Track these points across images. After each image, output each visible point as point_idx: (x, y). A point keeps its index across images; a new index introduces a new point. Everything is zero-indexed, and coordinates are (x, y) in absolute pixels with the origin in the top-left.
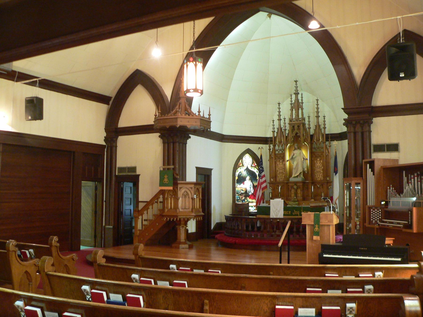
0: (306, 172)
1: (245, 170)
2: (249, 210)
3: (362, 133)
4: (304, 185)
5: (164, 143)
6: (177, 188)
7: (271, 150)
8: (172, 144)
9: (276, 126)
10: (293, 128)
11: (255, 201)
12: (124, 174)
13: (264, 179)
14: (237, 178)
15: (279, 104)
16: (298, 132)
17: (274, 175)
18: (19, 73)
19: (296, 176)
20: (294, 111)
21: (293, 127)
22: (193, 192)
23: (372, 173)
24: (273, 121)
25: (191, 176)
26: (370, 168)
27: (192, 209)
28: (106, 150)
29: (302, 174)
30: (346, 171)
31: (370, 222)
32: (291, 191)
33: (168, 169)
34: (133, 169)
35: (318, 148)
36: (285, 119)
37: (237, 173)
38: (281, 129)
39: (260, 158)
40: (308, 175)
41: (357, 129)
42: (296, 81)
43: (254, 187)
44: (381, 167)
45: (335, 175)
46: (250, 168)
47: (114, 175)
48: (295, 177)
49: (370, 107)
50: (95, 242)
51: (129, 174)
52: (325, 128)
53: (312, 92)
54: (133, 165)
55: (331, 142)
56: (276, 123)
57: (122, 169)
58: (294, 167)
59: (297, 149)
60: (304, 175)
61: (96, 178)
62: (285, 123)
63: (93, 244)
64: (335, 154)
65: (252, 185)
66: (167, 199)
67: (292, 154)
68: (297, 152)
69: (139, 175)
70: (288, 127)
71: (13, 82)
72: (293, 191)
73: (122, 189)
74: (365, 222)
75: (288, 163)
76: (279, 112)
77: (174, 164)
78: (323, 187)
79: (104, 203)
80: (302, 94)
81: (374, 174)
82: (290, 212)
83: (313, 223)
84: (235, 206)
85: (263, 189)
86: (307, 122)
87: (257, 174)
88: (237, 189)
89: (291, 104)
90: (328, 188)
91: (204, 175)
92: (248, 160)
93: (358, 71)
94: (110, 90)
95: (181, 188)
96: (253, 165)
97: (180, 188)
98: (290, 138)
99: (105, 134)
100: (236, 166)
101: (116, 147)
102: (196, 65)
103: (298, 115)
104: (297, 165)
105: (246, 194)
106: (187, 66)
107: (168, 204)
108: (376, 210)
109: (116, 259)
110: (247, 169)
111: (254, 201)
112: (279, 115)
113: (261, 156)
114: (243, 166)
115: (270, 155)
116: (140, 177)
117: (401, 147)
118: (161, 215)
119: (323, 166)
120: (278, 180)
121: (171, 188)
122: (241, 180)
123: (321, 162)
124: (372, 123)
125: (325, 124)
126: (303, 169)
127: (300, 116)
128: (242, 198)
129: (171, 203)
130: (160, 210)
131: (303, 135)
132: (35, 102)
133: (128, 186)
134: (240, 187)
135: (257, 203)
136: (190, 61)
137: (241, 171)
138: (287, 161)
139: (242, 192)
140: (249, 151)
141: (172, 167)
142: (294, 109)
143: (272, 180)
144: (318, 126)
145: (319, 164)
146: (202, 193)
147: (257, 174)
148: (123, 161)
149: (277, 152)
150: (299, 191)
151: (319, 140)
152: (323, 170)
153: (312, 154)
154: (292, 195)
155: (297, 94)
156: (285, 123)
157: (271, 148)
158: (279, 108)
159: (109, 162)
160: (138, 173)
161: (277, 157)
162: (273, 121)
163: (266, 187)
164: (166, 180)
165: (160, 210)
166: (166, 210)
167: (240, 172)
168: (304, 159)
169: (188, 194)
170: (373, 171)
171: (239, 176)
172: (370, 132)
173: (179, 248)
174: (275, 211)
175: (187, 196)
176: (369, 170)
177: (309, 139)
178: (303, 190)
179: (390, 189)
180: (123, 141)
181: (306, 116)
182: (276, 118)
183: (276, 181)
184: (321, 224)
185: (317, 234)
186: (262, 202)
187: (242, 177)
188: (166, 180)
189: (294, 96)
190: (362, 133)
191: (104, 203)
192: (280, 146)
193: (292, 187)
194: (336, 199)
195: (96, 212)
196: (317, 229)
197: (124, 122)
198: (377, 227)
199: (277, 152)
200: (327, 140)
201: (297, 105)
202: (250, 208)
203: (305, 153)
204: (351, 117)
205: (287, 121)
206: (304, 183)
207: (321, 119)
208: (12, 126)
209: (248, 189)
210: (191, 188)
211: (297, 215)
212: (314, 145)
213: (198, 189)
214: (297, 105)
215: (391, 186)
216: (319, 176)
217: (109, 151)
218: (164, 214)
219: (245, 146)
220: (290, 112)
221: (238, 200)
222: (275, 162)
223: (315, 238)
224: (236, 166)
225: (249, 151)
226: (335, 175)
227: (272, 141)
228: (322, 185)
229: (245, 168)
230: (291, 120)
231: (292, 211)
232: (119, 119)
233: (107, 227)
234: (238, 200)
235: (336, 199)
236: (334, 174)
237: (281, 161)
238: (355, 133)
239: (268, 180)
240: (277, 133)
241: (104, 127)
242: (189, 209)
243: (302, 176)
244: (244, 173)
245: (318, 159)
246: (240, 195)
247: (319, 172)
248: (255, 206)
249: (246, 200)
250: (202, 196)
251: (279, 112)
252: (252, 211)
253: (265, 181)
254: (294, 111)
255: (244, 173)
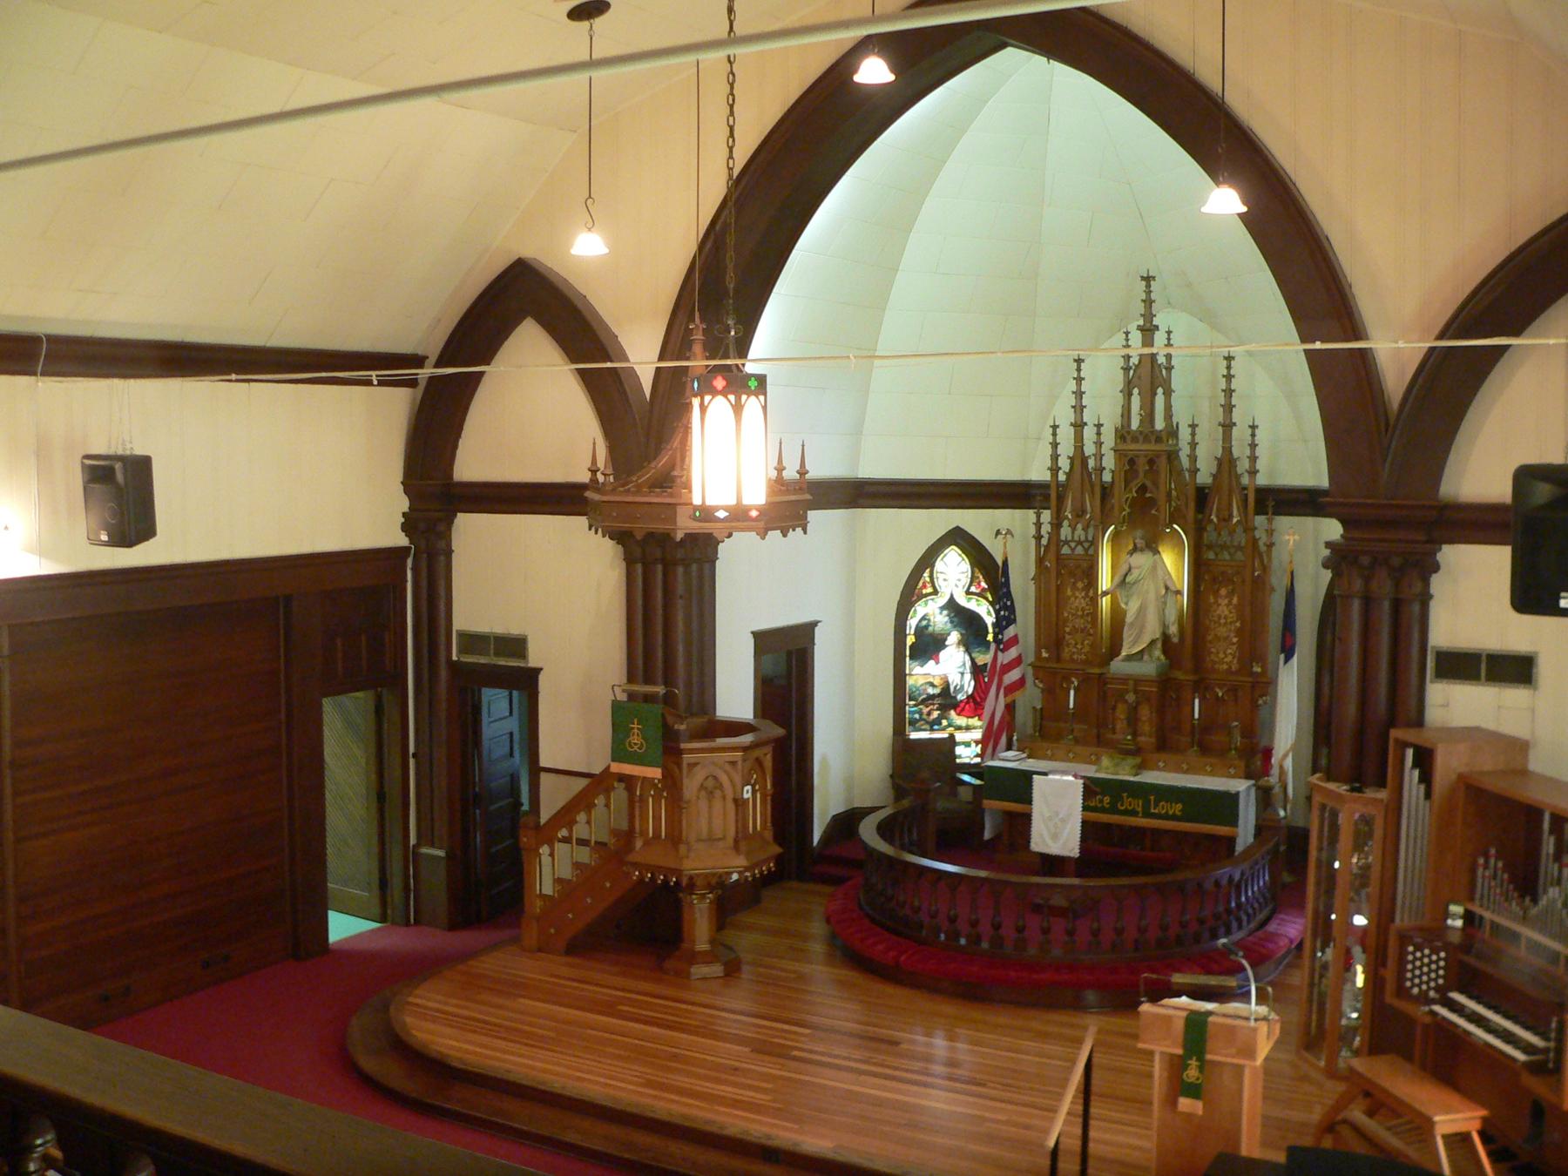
0: (1175, 640)
1: (942, 608)
2: (955, 757)
3: (1397, 606)
4: (1166, 691)
5: (629, 560)
6: (679, 765)
7: (1044, 541)
8: (660, 567)
9: (1066, 449)
10: (1128, 464)
11: (979, 723)
12: (483, 660)
13: (1013, 653)
14: (910, 640)
15: (1079, 361)
16: (1148, 484)
17: (1052, 635)
18: (50, 338)
19: (1137, 659)
20: (1136, 401)
21: (1132, 462)
22: (738, 779)
23: (1422, 787)
24: (1055, 427)
25: (735, 694)
26: (1415, 765)
27: (736, 841)
28: (409, 562)
29: (1159, 645)
30: (1329, 638)
31: (1402, 992)
32: (1114, 708)
33: (648, 698)
34: (516, 645)
35: (1224, 547)
36: (1099, 426)
37: (912, 623)
38: (1084, 460)
39: (1000, 563)
40: (1185, 649)
41: (1374, 585)
42: (1148, 279)
43: (977, 671)
44: (1461, 777)
45: (1286, 661)
46: (962, 600)
47: (443, 659)
48: (1129, 658)
49: (1431, 508)
50: (384, 903)
51: (502, 662)
52: (1253, 472)
53: (1209, 317)
54: (514, 630)
55: (1278, 518)
56: (1066, 436)
57: (473, 641)
58: (1129, 618)
59: (1142, 550)
60: (1165, 652)
61: (381, 676)
62: (1099, 444)
63: (376, 910)
64: (1286, 581)
65: (968, 664)
66: (643, 800)
67: (1125, 568)
68: (1142, 560)
69: (537, 671)
70: (1109, 462)
71: (33, 378)
72: (1121, 712)
73: (477, 709)
74: (1384, 965)
75: (1105, 602)
76: (1079, 394)
77: (668, 681)
78: (1236, 701)
79: (412, 761)
80: (1169, 333)
81: (1428, 795)
82: (1107, 799)
83: (1180, 1051)
84: (904, 751)
85: (1011, 689)
86: (1184, 453)
87: (990, 620)
88: (910, 681)
89: (1126, 369)
90: (1255, 706)
91: (787, 661)
92: (953, 570)
93: (1397, 346)
94: (417, 319)
95: (696, 764)
96: (973, 589)
97: (692, 765)
98: (1122, 499)
99: (404, 504)
100: (910, 595)
101: (449, 552)
102: (738, 409)
103: (1149, 416)
104: (1142, 610)
105: (946, 699)
106: (703, 409)
107: (644, 819)
108: (1427, 951)
109: (450, 1068)
110: (952, 605)
111: (975, 721)
112: (1079, 408)
113: (1005, 562)
114: (935, 592)
115: (1040, 561)
116: (542, 678)
117: (1543, 670)
118: (616, 851)
119: (1241, 617)
120: (1066, 654)
121: (655, 773)
122: (928, 646)
123: (1235, 600)
124: (1436, 568)
125: (1253, 459)
126: (1165, 626)
127: (1160, 424)
128: (929, 714)
129: (657, 818)
130: (615, 833)
131: (1169, 494)
132: (120, 477)
133: (496, 702)
134: (922, 675)
135: (983, 742)
136: (714, 392)
137: (930, 611)
138: (1105, 594)
139: (931, 691)
140: (958, 537)
141: (660, 690)
142: (1136, 391)
143: (1045, 655)
144: (1226, 462)
145: (1224, 608)
146: (775, 769)
147: (990, 620)
148: (477, 605)
149: (1065, 550)
150: (1145, 713)
151: (1231, 516)
152: (1239, 632)
153: (1199, 568)
154: (1119, 726)
155: (1148, 331)
156: (1099, 444)
157: (1043, 532)
158: (1079, 380)
159: (424, 609)
160: (533, 662)
161: (1066, 570)
162: (1055, 427)
163: (1021, 683)
164: (636, 739)
165: (615, 833)
166: (639, 844)
167: (923, 618)
168: (1167, 588)
169: (721, 787)
170: (1426, 778)
171: (920, 631)
172: (1425, 598)
173: (688, 976)
174: (1050, 819)
175: (718, 793)
176: (1412, 776)
177: (1191, 513)
178: (1161, 711)
179: (1486, 866)
180: (473, 532)
181: (1182, 418)
182: (1065, 417)
183: (1059, 659)
184: (1209, 1057)
185: (1194, 1091)
186: (1004, 739)
187: (932, 635)
188: (636, 739)
189: (1136, 337)
190: (1397, 606)
191: (412, 761)
192: (1079, 526)
193: (1121, 696)
194: (1285, 756)
195: (381, 797)
196: (1192, 1074)
197: (475, 461)
198: (1428, 1020)
199: (1065, 550)
200: (1261, 509)
201: (1148, 377)
202: (959, 750)
203: (1174, 563)
204: (1357, 534)
205: (1109, 439)
206: (1165, 682)
207: (1240, 434)
208: (42, 552)
209: (954, 680)
210: (733, 763)
211: (1134, 813)
212: (1210, 536)
213: (759, 762)
214: (1148, 377)
215: (1493, 851)
216: (1225, 656)
217: (424, 565)
218: (631, 858)
219: (943, 519)
220: (1120, 398)
221: (917, 721)
222: (1058, 587)
223: (1185, 1103)
224: (910, 595)
225: (958, 537)
226: (1286, 661)
227: (1047, 497)
228: (1233, 690)
229: (942, 600)
230: (1123, 434)
231: (1116, 798)
232: (455, 447)
233: (424, 850)
234: (913, 723)
235: (1285, 756)
236: (1282, 657)
237: (1080, 585)
238: (1368, 602)
239: (1030, 658)
240: (1069, 475)
241: (400, 477)
242: (724, 838)
243: (1158, 653)
244: (940, 621)
245: (1223, 592)
246: (923, 702)
247: (1226, 638)
248: (977, 743)
249: (945, 722)
250: (774, 785)
251: (1079, 394)
252: (967, 761)
253: (1018, 661)
254: (1136, 401)
255: (940, 621)
